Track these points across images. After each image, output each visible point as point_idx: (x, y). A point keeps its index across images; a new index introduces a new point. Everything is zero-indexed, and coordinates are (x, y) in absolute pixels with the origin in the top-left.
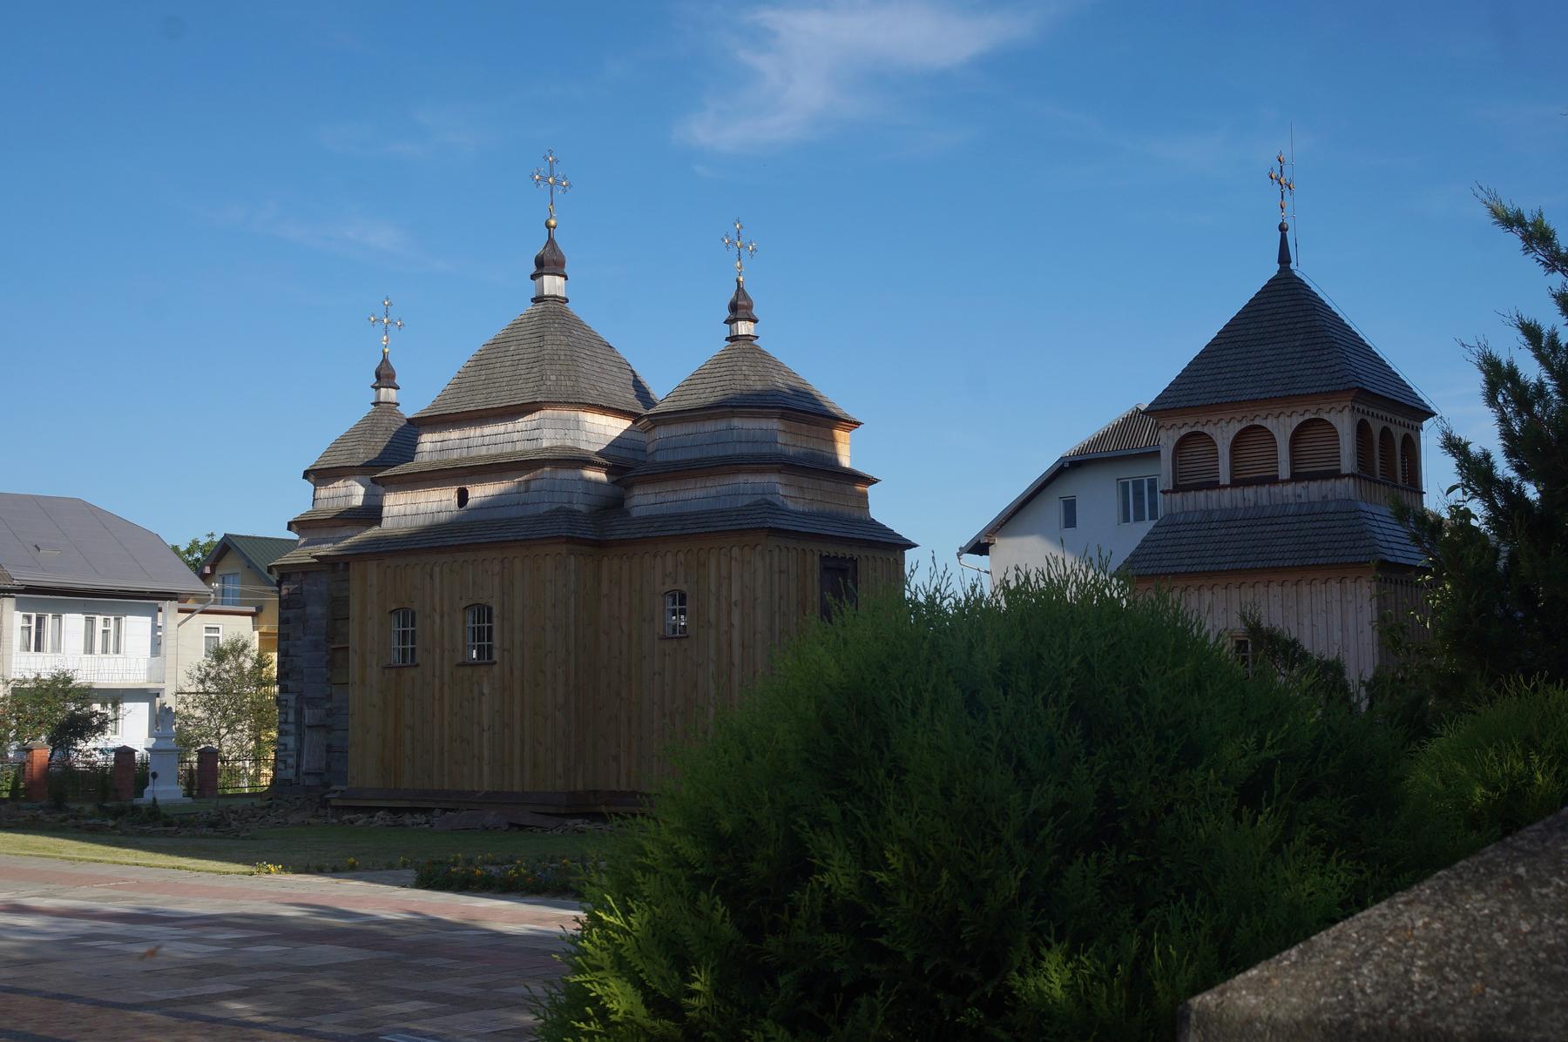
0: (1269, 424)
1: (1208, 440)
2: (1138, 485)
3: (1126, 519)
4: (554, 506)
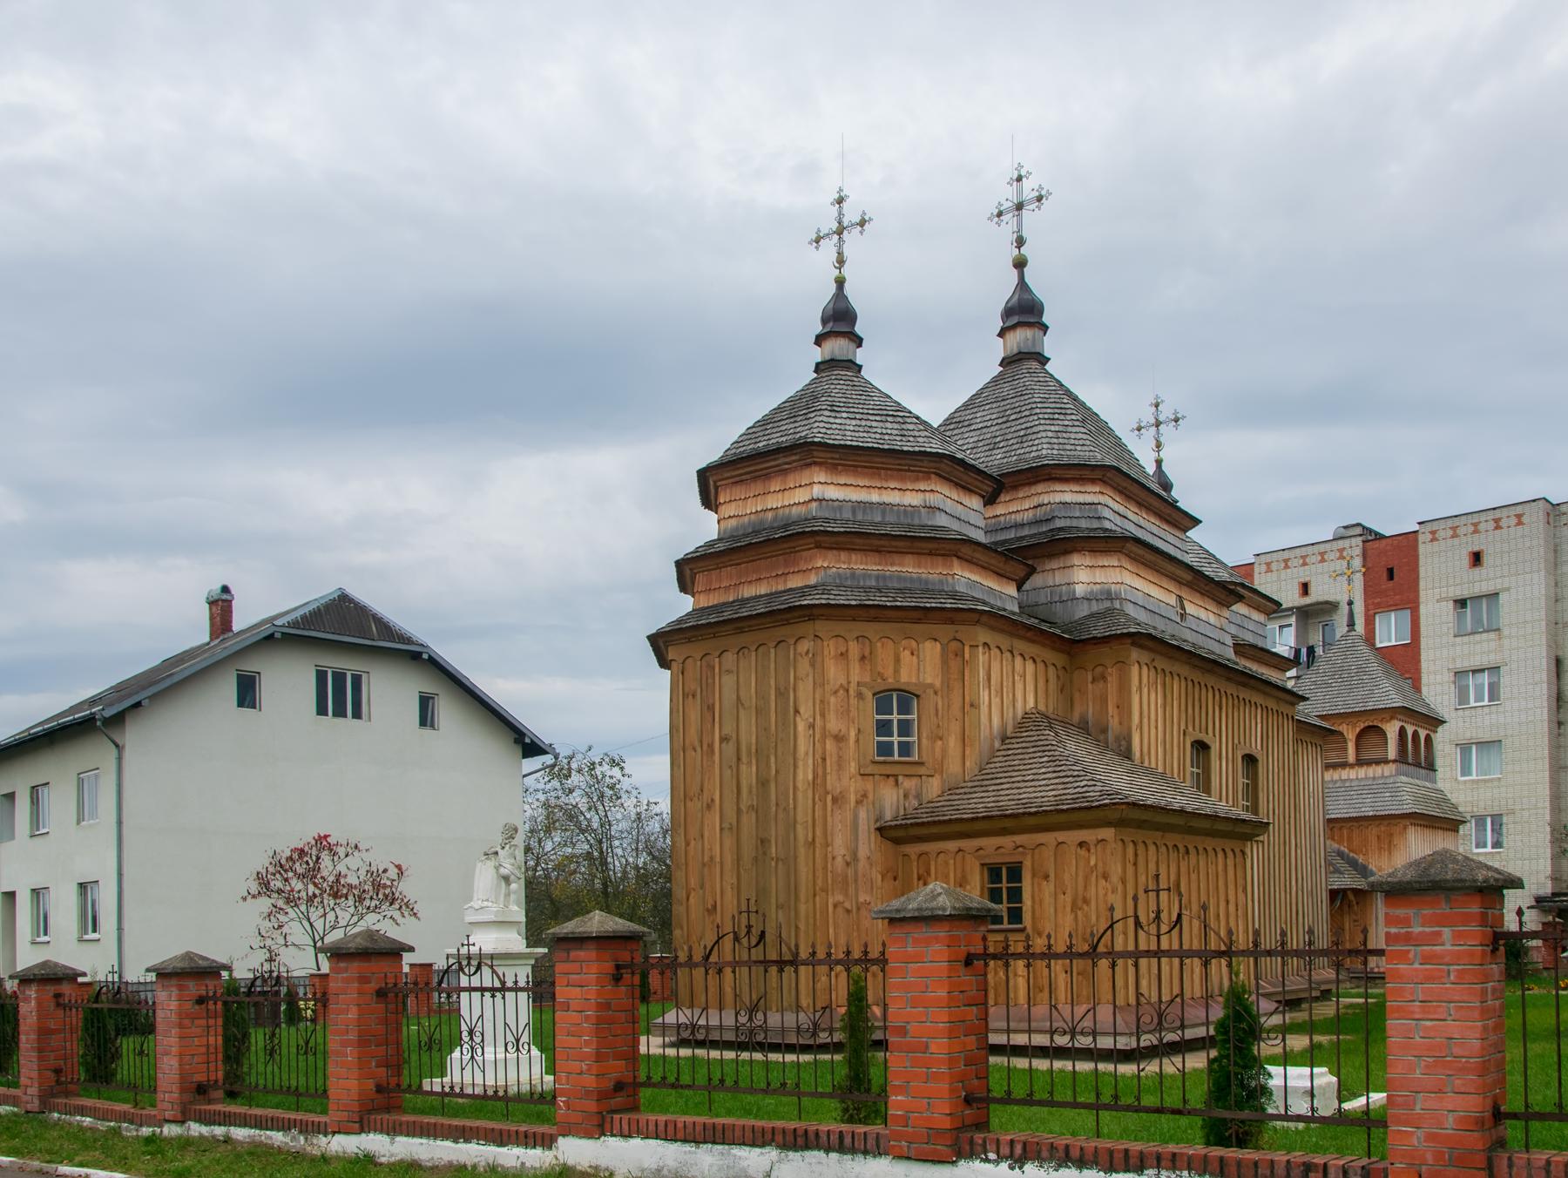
0: (1343, 728)
1: (1383, 734)
2: (339, 678)
3: (322, 710)
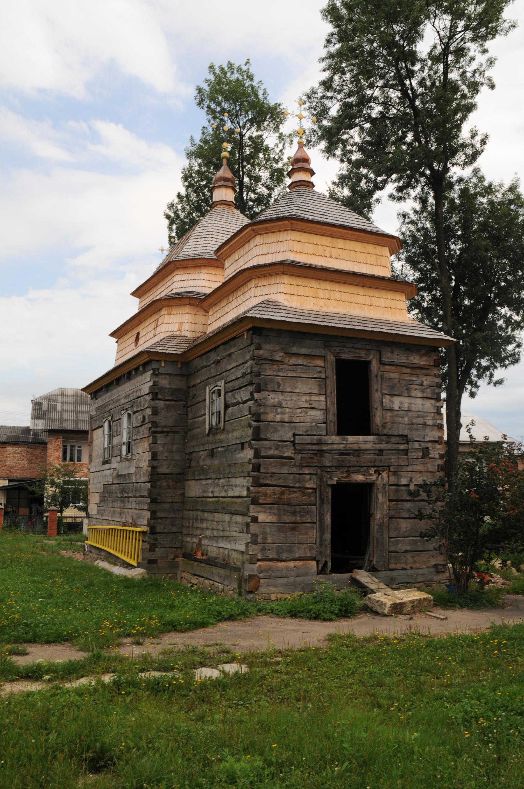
4: (168, 334)
